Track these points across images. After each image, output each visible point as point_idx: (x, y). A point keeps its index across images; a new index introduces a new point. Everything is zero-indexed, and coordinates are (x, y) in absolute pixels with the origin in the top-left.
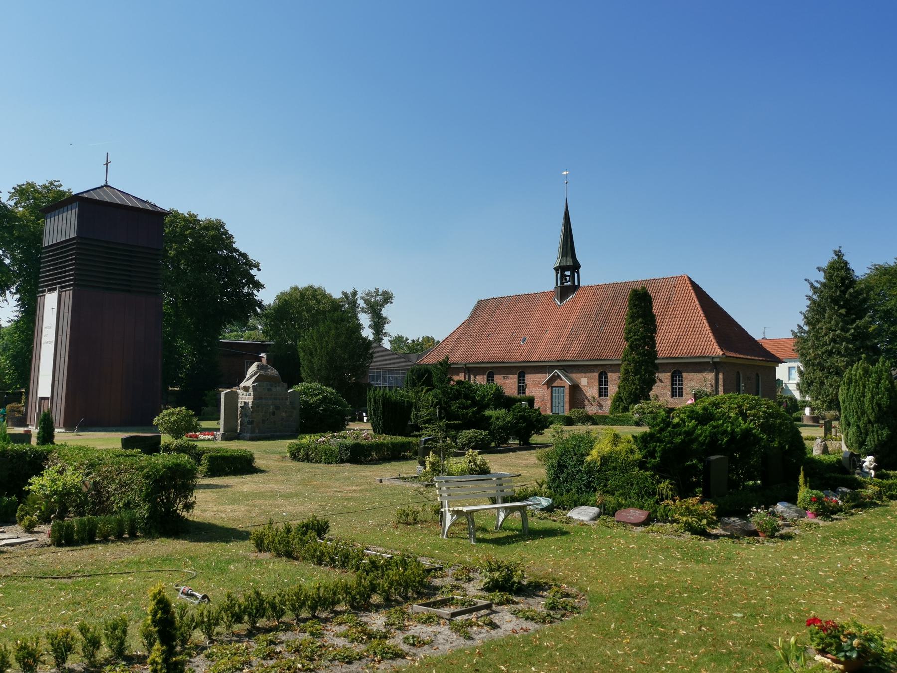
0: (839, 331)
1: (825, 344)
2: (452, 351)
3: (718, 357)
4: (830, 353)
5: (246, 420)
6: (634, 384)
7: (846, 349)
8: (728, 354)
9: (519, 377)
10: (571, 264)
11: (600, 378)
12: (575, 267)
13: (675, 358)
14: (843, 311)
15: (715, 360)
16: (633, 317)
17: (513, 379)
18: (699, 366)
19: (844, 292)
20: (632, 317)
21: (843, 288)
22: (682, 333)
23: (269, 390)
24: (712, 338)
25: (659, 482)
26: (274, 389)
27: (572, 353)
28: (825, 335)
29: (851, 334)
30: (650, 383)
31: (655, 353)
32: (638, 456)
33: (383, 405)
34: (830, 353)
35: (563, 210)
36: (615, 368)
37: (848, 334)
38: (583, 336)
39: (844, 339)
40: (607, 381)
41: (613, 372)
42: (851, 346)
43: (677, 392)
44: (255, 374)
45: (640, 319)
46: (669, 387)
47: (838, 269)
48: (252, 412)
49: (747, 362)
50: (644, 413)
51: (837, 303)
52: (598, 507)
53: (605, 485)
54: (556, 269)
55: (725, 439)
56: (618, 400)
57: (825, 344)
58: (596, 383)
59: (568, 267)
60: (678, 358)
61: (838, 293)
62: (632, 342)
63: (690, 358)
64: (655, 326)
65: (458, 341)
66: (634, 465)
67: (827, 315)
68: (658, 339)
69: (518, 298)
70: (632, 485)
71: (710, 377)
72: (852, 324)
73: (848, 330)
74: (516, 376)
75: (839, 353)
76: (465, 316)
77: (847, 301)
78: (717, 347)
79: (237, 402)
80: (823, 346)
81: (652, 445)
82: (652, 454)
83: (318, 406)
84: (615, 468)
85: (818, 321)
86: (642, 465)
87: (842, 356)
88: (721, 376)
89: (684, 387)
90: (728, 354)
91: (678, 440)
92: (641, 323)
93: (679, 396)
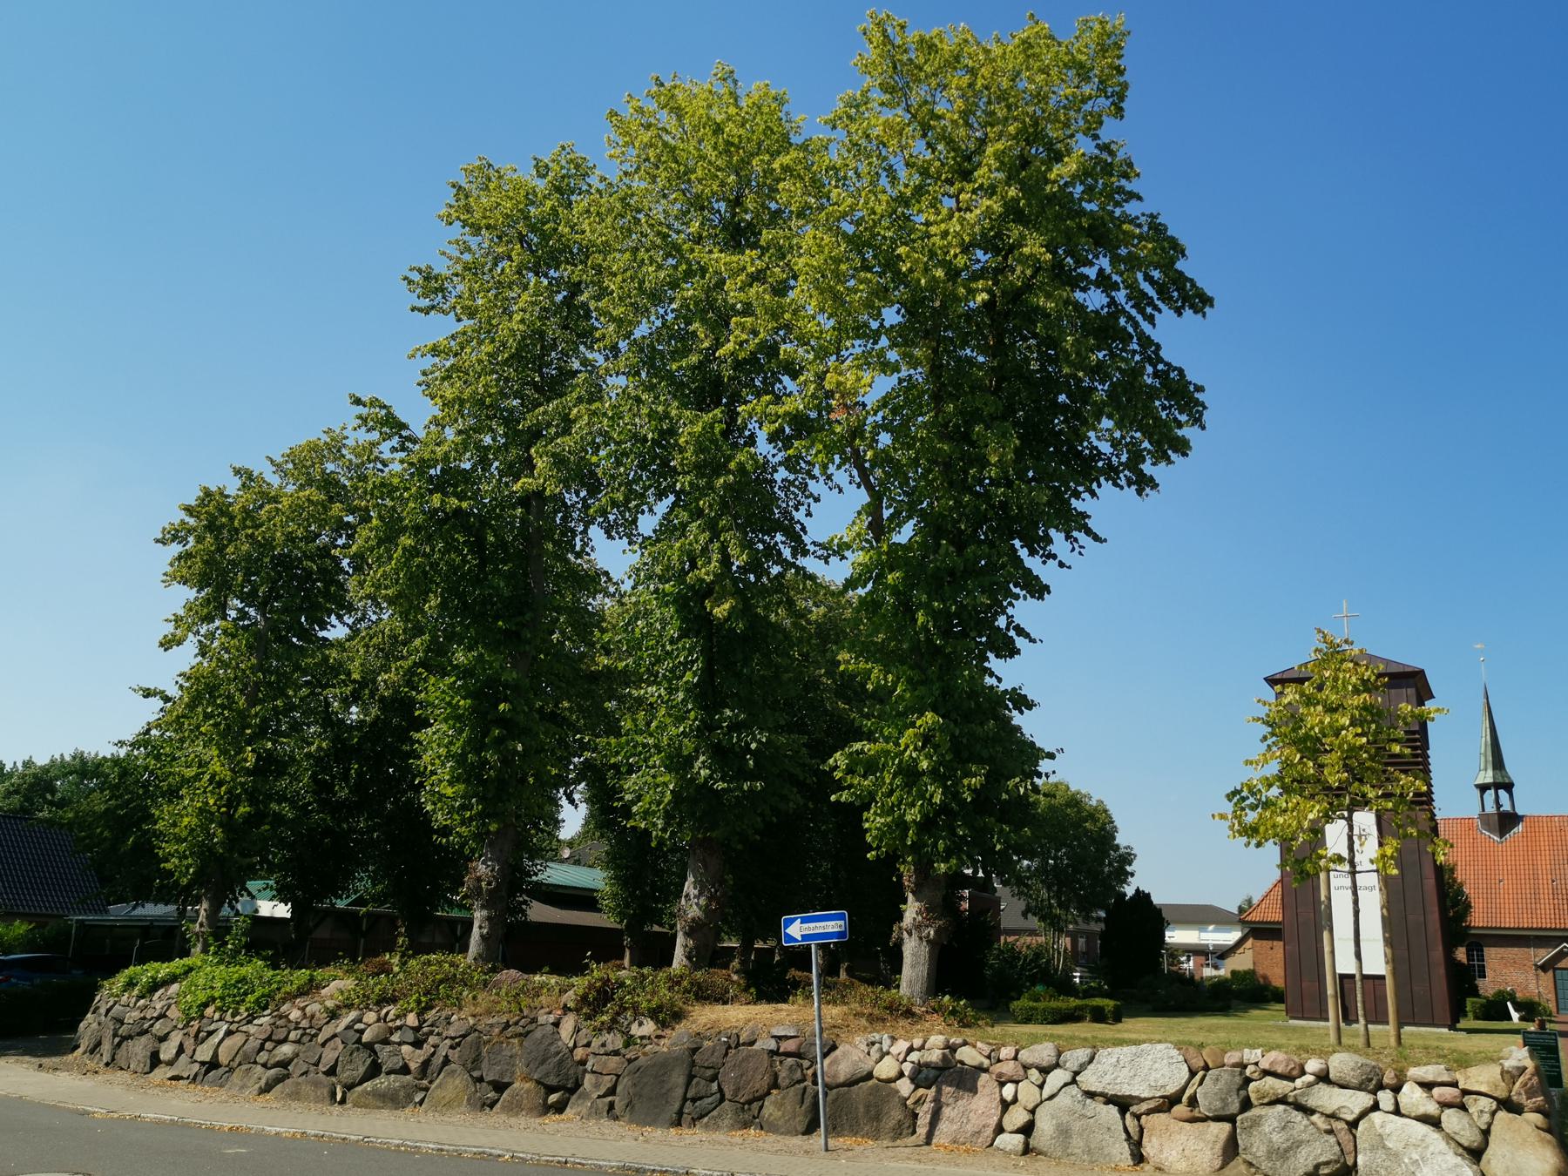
12: (1509, 787)
54: (1483, 788)
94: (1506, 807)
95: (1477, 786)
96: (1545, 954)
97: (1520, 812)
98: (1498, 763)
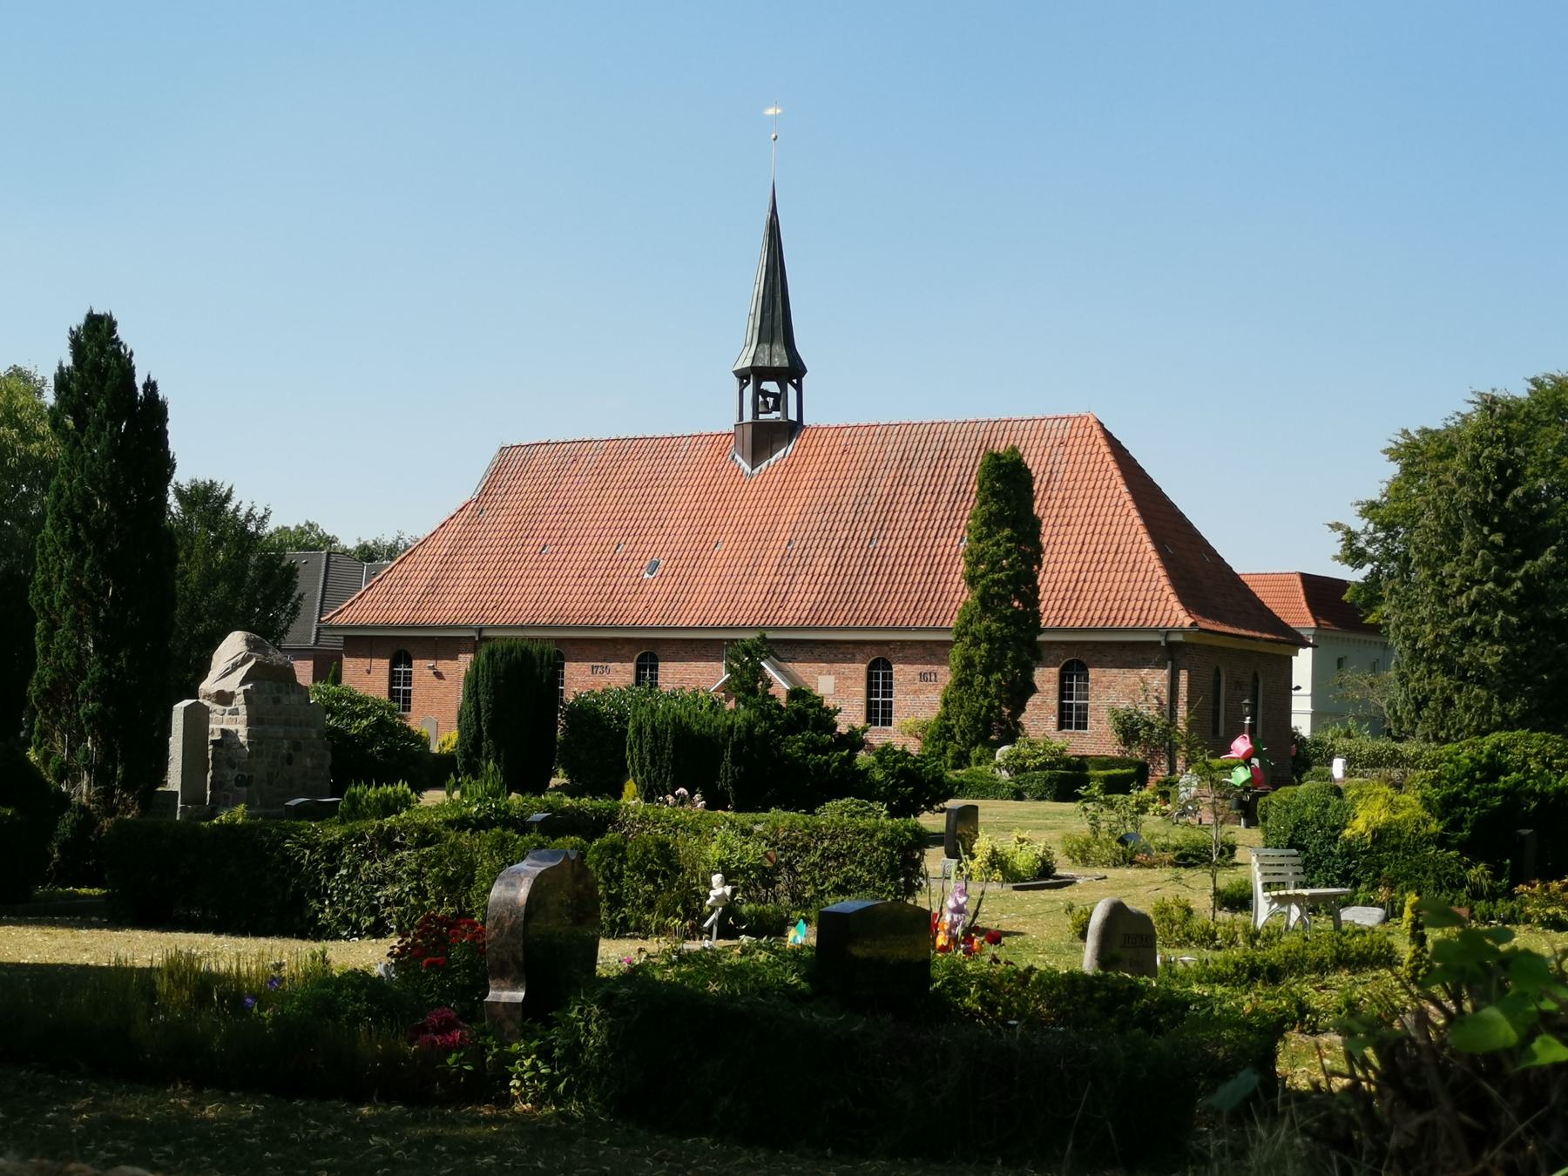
0: (1490, 585)
1: (1458, 613)
2: (433, 589)
3: (1182, 630)
4: (1467, 634)
5: (231, 774)
6: (986, 695)
7: (1504, 624)
8: (1206, 624)
9: (639, 668)
10: (786, 363)
11: (870, 676)
12: (794, 372)
13: (1073, 630)
14: (1497, 538)
15: (1173, 638)
16: (991, 523)
17: (382, 665)
18: (1130, 651)
19: (1502, 495)
20: (985, 523)
21: (1499, 486)
22: (1096, 572)
23: (277, 701)
24: (1164, 581)
25: (1468, 866)
26: (285, 700)
27: (796, 610)
28: (1460, 592)
29: (1516, 593)
30: (1022, 691)
31: (1037, 616)
32: (1435, 827)
33: (676, 742)
34: (1467, 634)
35: (767, 214)
36: (930, 651)
37: (1507, 592)
38: (823, 563)
39: (1502, 603)
40: (888, 686)
41: (906, 661)
42: (1514, 620)
43: (1071, 717)
44: (245, 661)
45: (1007, 532)
46: (1054, 704)
47: (1491, 442)
48: (250, 755)
49: (1246, 646)
50: (1023, 769)
51: (1485, 521)
52: (1381, 905)
53: (1378, 875)
54: (742, 376)
55: (1533, 805)
56: (941, 736)
57: (1458, 613)
58: (861, 689)
59: (777, 368)
60: (1081, 630)
61: (1490, 497)
62: (986, 588)
63: (1112, 630)
64: (1039, 550)
65: (449, 562)
66: (1428, 843)
67: (1464, 546)
68: (1045, 580)
69: (626, 449)
70: (1425, 873)
71: (1157, 678)
72: (1515, 568)
73: (1510, 582)
74: (631, 667)
75: (1487, 634)
76: (467, 490)
77: (1505, 515)
78: (1178, 606)
79: (206, 733)
80: (1452, 618)
81: (1459, 810)
82: (1456, 825)
83: (371, 744)
84: (1396, 848)
85: (1442, 559)
86: (1441, 841)
87: (1494, 642)
88: (1183, 677)
89: (1091, 703)
90: (1206, 624)
91: (1497, 801)
92: (1009, 539)
93: (1078, 727)
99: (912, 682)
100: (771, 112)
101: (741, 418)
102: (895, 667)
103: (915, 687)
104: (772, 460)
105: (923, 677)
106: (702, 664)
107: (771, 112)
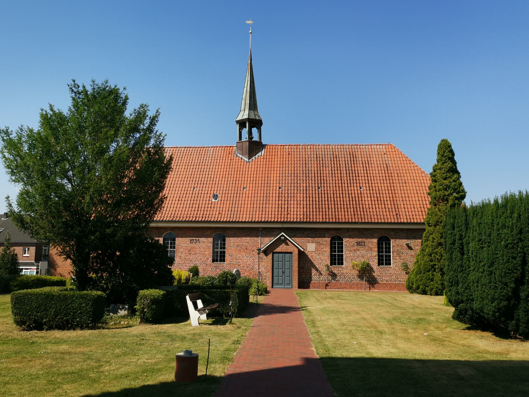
17: (205, 245)
27: (296, 214)
38: (300, 196)
41: (350, 237)
54: (242, 124)
58: (328, 249)
74: (211, 240)
93: (339, 264)
94: (256, 138)
95: (237, 122)
96: (268, 241)
97: (264, 142)
98: (253, 106)
99: (353, 246)
100: (249, 22)
101: (240, 138)
102: (345, 240)
103: (355, 248)
104: (257, 156)
105: (358, 244)
106: (248, 238)
107: (249, 22)
